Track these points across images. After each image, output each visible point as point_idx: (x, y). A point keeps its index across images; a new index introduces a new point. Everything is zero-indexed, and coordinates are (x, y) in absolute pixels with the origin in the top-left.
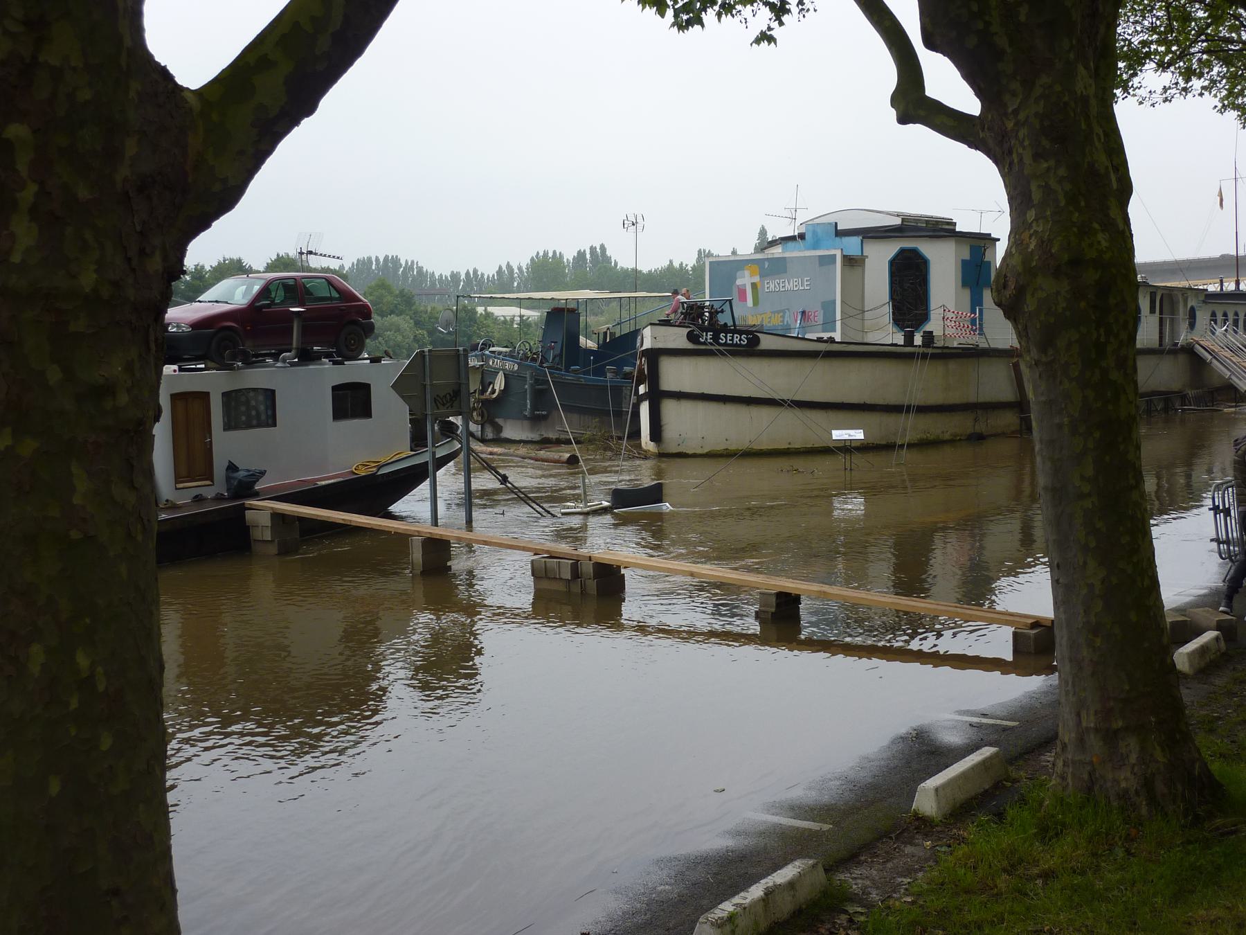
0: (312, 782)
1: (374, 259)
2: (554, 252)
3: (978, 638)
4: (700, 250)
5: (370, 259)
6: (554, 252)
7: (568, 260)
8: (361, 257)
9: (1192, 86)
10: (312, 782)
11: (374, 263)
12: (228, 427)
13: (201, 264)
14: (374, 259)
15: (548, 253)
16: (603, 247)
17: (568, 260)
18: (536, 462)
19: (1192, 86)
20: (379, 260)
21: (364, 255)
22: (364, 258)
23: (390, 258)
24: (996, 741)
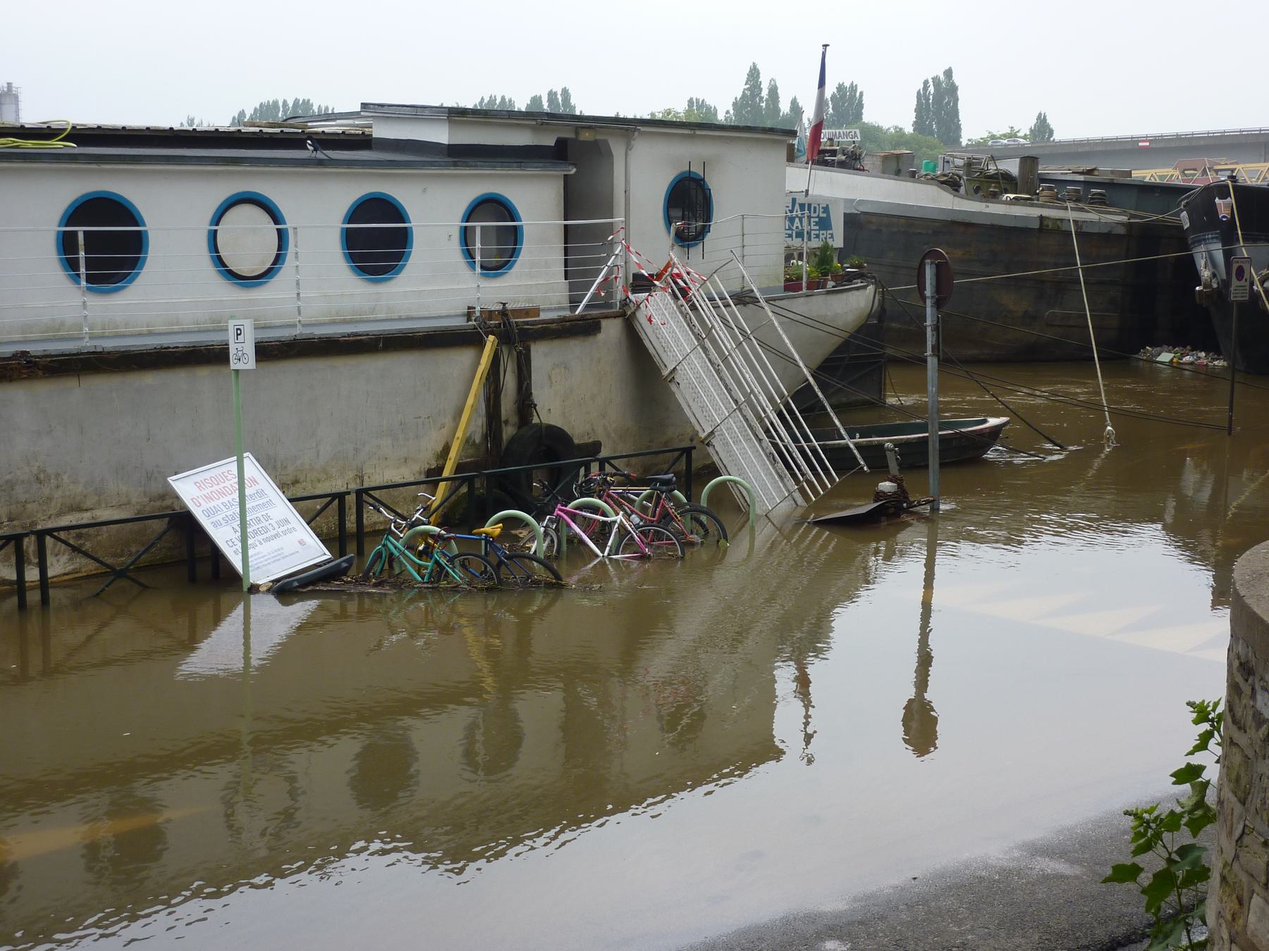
0: (458, 884)
1: (281, 104)
2: (503, 98)
3: (1016, 565)
4: (691, 99)
5: (275, 103)
6: (503, 98)
7: (794, 104)
8: (264, 100)
9: (415, 791)
10: (458, 884)
11: (281, 109)
12: (539, 316)
13: (554, 91)
14: (281, 104)
15: (496, 100)
16: (565, 92)
17: (794, 104)
18: (919, 231)
19: (415, 791)
20: (505, 99)
21: (268, 97)
22: (268, 101)
23: (301, 102)
24: (981, 877)
